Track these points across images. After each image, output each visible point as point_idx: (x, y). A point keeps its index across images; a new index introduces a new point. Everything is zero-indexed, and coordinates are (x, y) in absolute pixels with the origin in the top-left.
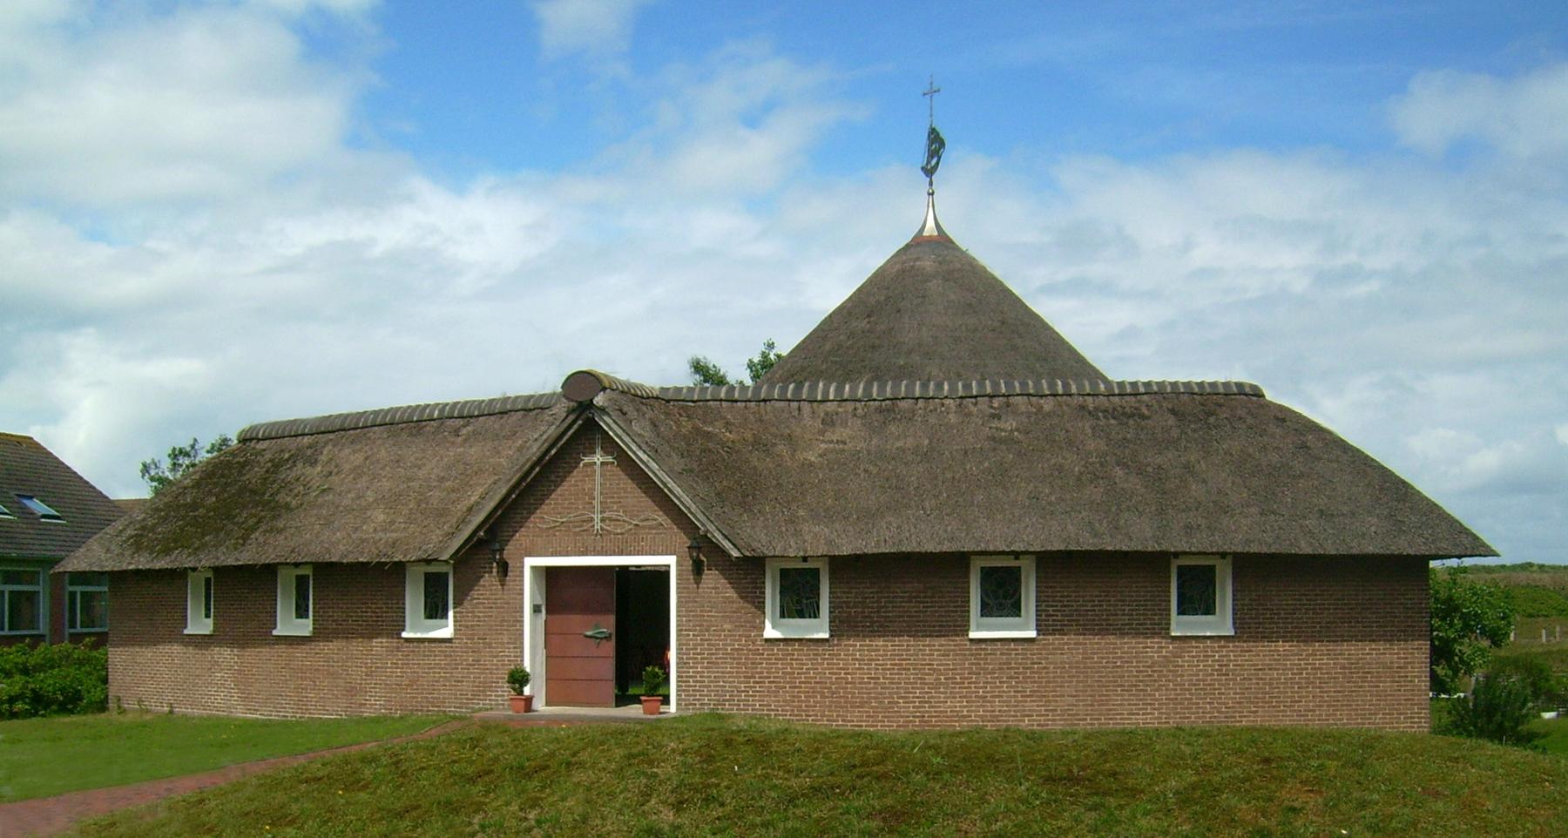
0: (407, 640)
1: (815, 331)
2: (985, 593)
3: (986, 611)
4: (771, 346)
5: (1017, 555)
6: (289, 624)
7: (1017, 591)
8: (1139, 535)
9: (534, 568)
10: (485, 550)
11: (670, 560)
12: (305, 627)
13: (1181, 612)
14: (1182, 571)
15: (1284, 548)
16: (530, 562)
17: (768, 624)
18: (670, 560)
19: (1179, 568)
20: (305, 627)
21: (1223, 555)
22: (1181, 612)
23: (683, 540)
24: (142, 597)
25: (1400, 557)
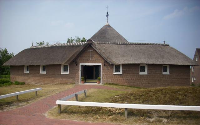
0: (41, 74)
1: (97, 33)
2: (115, 68)
3: (116, 71)
4: (71, 37)
5: (120, 64)
6: (42, 72)
7: (120, 68)
8: (160, 62)
9: (82, 65)
10: (74, 62)
11: (101, 64)
12: (28, 72)
13: (164, 72)
14: (141, 66)
15: (176, 64)
16: (80, 64)
17: (114, 72)
18: (101, 64)
19: (84, 67)
20: (45, 73)
21: (146, 64)
22: (164, 72)
23: (103, 61)
24: (19, 68)
25: (136, 64)
